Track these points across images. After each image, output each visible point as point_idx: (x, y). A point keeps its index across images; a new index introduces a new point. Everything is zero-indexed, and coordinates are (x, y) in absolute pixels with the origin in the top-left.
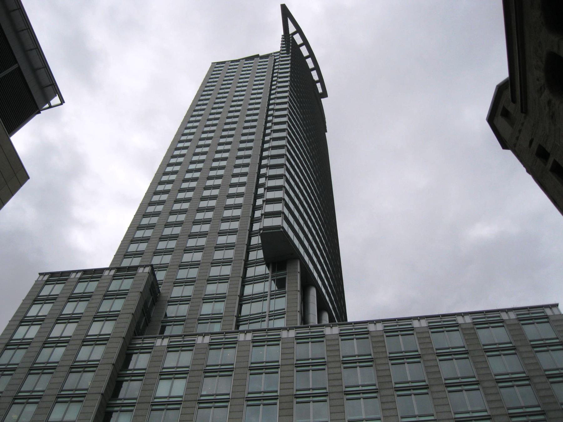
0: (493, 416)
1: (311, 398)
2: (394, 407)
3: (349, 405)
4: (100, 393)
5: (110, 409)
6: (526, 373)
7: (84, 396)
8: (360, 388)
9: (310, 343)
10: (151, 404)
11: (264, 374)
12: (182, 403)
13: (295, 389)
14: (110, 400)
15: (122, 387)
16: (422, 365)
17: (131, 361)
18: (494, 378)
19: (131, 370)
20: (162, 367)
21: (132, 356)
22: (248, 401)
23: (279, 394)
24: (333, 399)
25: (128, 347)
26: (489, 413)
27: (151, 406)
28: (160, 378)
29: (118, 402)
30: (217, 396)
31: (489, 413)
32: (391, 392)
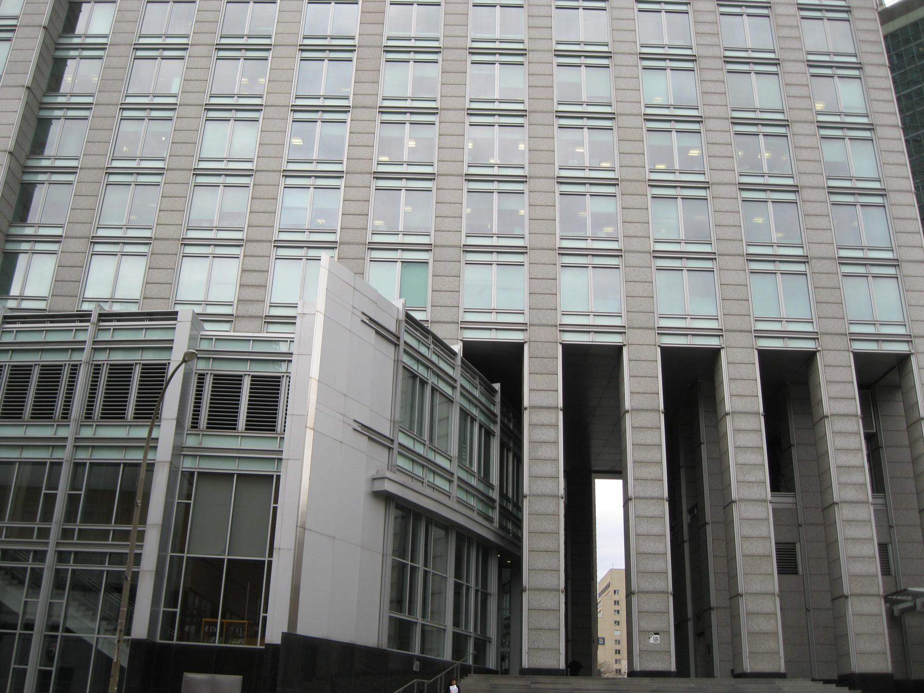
0: (700, 57)
1: (408, 115)
2: (548, 26)
3: (471, 275)
4: (41, 26)
5: (11, 247)
6: (776, 52)
7: (13, 31)
8: (497, 106)
9: (407, 125)
10: (133, 47)
11: (326, 62)
12: (188, 49)
13: (381, 96)
14: (60, 37)
15: (81, 11)
16: (621, 276)
17: (81, 13)
18: (730, 115)
19: (79, 36)
20: (139, 33)
21: (81, 6)
22: (303, 50)
23: (357, 43)
24: (450, 3)
25: (8, 235)
26: (707, 178)
27: (135, 51)
28: (135, 56)
29: (29, 231)
30: (249, 39)
31: (707, 178)
32: (552, 256)
